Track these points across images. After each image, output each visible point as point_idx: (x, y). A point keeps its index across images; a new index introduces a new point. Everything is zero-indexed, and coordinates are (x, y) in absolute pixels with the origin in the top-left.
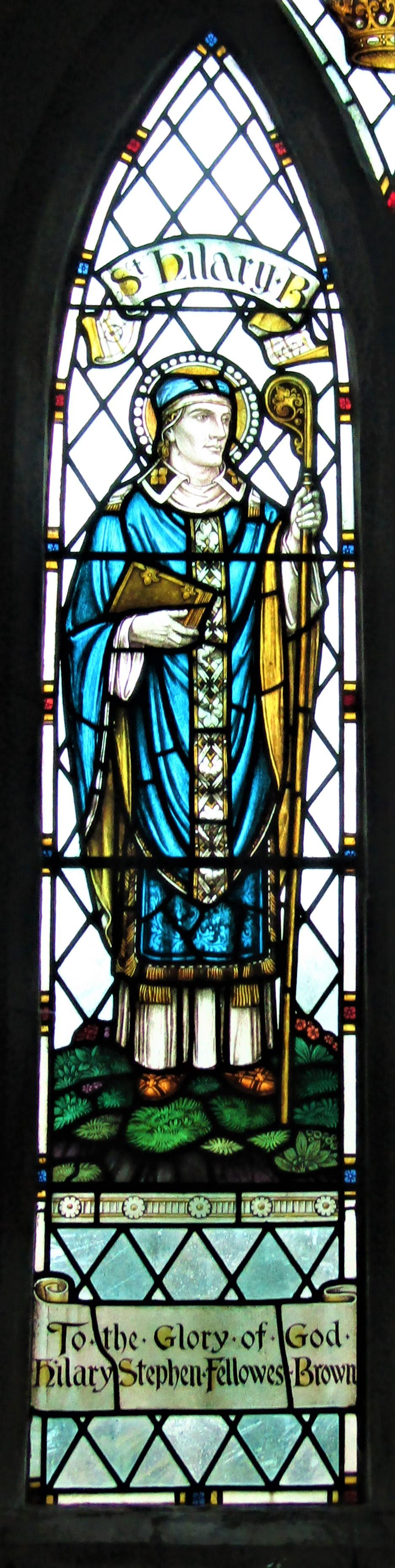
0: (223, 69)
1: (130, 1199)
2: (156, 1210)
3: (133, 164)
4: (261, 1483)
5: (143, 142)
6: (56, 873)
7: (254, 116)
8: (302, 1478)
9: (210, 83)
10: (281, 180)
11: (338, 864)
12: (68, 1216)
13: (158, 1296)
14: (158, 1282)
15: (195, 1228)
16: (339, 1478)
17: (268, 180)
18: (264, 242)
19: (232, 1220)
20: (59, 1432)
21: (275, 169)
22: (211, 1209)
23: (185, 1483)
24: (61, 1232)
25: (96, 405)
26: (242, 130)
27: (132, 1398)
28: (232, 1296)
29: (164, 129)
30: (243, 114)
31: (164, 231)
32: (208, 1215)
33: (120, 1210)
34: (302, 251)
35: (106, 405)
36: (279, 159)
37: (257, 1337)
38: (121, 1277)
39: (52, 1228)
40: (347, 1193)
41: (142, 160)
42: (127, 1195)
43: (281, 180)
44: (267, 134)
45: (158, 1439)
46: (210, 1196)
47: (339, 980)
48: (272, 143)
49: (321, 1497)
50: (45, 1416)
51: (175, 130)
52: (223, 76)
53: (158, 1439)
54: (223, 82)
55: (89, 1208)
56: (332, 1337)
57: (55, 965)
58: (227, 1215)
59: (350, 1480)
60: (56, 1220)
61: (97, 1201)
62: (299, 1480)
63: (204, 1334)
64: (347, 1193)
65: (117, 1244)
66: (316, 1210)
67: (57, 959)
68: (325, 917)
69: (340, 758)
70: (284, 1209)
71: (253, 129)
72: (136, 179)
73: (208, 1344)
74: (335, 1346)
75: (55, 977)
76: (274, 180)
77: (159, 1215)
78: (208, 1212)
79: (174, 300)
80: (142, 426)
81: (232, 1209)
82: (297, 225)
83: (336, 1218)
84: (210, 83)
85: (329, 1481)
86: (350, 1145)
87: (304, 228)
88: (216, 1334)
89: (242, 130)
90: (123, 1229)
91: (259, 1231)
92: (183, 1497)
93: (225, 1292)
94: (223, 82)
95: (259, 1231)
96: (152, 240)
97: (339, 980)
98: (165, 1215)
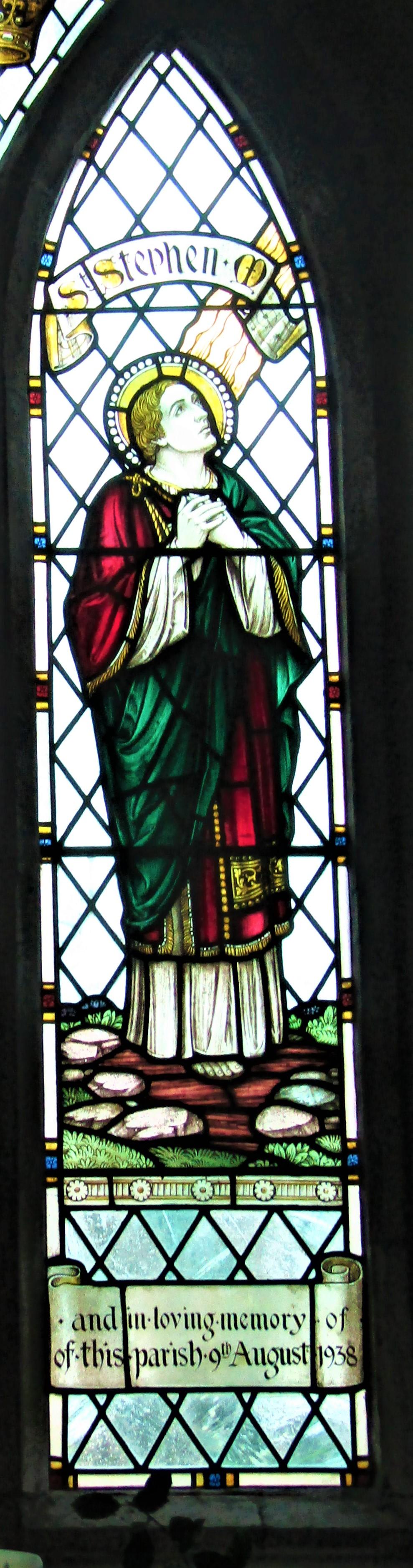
0: (174, 65)
1: (199, 1182)
2: (285, 1193)
3: (91, 162)
4: (131, 1466)
5: (101, 138)
6: (56, 862)
7: (210, 110)
8: (306, 1462)
9: (162, 80)
10: (244, 172)
11: (329, 850)
12: (74, 1198)
13: (170, 1276)
14: (241, 1263)
15: (204, 1211)
16: (353, 1461)
17: (230, 173)
18: (221, 233)
19: (227, 1202)
20: (82, 1411)
21: (236, 161)
22: (151, 1191)
23: (206, 1465)
24: (74, 1214)
25: (274, 407)
26: (199, 125)
27: (148, 1376)
28: (170, 1276)
29: (120, 127)
30: (199, 109)
32: (272, 1198)
33: (252, 1194)
34: (271, 242)
35: (278, 406)
36: (241, 151)
37: (339, 1319)
38: (134, 1258)
40: (350, 1178)
41: (101, 158)
42: (135, 1178)
43: (244, 172)
44: (226, 129)
46: (273, 1178)
47: (336, 964)
48: (233, 137)
49: (335, 1480)
50: (65, 1393)
51: (132, 126)
52: (174, 71)
54: (174, 78)
55: (226, 1191)
56: (109, 1322)
57: (59, 951)
58: (221, 1197)
59: (363, 1465)
60: (68, 1203)
61: (233, 1184)
62: (114, 1465)
63: (284, 1316)
64: (350, 1178)
65: (270, 1225)
66: (193, 1193)
67: (61, 945)
68: (320, 902)
69: (326, 742)
70: (180, 1192)
71: (210, 123)
72: (96, 182)
73: (287, 1325)
74: (112, 1329)
75: (59, 965)
76: (236, 173)
77: (165, 1197)
78: (272, 1193)
79: (141, 298)
80: (227, 426)
81: (240, 1191)
82: (265, 216)
83: (340, 1203)
84: (162, 80)
85: (342, 1464)
86: (352, 1131)
87: (272, 218)
88: (296, 1317)
89: (199, 125)
90: (135, 1211)
91: (264, 1213)
93: (234, 1272)
94: (174, 78)
95: (264, 1213)
96: (121, 237)
97: (336, 964)
98: (177, 1197)
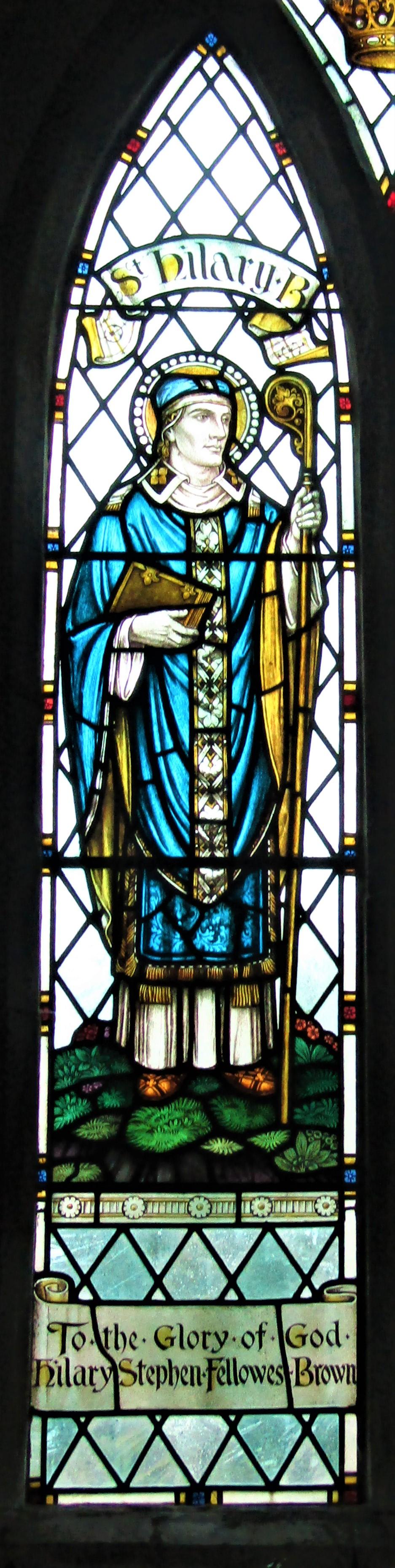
0: (223, 69)
1: (130, 1199)
2: (156, 1210)
3: (133, 164)
4: (261, 1483)
5: (143, 142)
7: (254, 116)
8: (302, 1478)
9: (210, 83)
10: (281, 180)
11: (338, 864)
12: (68, 1216)
13: (158, 1296)
14: (158, 1282)
15: (195, 1228)
16: (339, 1478)
17: (268, 180)
18: (264, 242)
19: (232, 1220)
20: (59, 1432)
21: (275, 169)
22: (211, 1209)
23: (185, 1483)
24: (61, 1232)
25: (96, 405)
26: (242, 130)
27: (132, 1398)
28: (232, 1296)
29: (164, 129)
30: (243, 114)
32: (208, 1215)
33: (120, 1210)
34: (302, 251)
35: (106, 405)
36: (279, 159)
37: (257, 1337)
38: (121, 1277)
40: (347, 1193)
41: (142, 160)
42: (127, 1195)
43: (281, 180)
44: (267, 134)
45: (158, 1439)
46: (210, 1196)
47: (339, 980)
48: (272, 143)
49: (321, 1497)
50: (45, 1416)
51: (175, 130)
52: (223, 76)
53: (158, 1439)
54: (223, 82)
55: (89, 1208)
56: (332, 1337)
57: (55, 965)
58: (227, 1215)
59: (350, 1480)
60: (56, 1220)
61: (97, 1201)
62: (299, 1480)
63: (204, 1334)
64: (347, 1193)
65: (117, 1244)
66: (316, 1210)
67: (57, 959)
68: (325, 917)
69: (340, 758)
70: (284, 1209)
71: (253, 129)
73: (208, 1344)
74: (335, 1346)
76: (274, 180)
77: (159, 1215)
78: (208, 1212)
81: (232, 1209)
82: (297, 225)
83: (336, 1218)
84: (210, 83)
85: (329, 1481)
86: (350, 1145)
87: (304, 228)
88: (216, 1334)
89: (242, 130)
90: (123, 1229)
91: (259, 1231)
93: (225, 1292)
94: (223, 82)
95: (259, 1231)
96: (152, 240)
97: (339, 980)
98: (165, 1215)
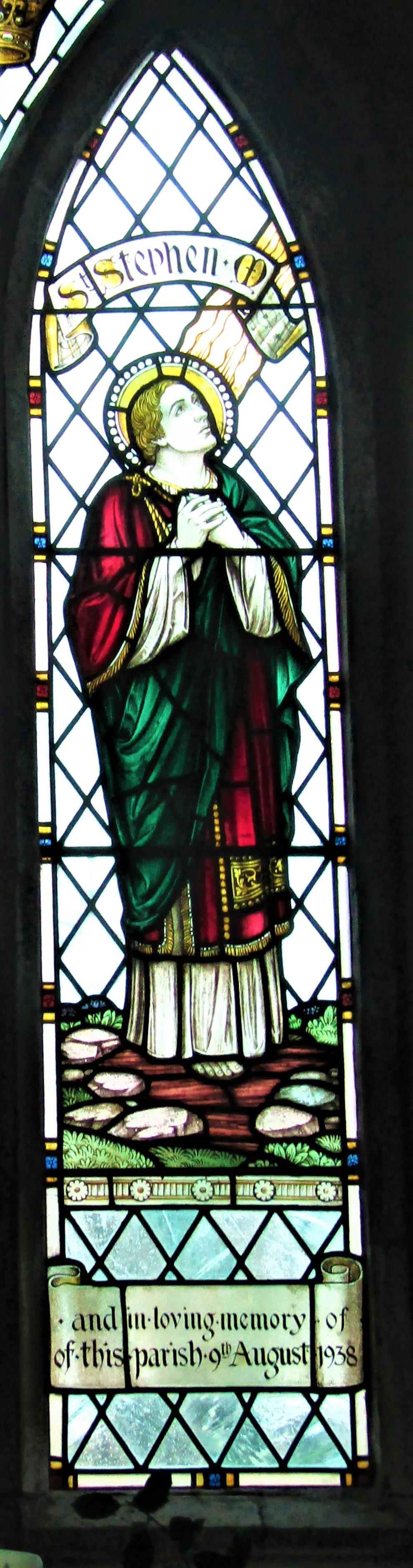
0: (174, 65)
1: (199, 1182)
2: (285, 1193)
3: (91, 162)
4: (131, 1466)
5: (101, 138)
6: (56, 862)
7: (210, 110)
8: (306, 1462)
9: (162, 80)
10: (244, 172)
11: (329, 850)
12: (74, 1198)
13: (170, 1276)
14: (241, 1263)
15: (204, 1211)
16: (353, 1461)
17: (230, 173)
18: (221, 233)
19: (227, 1202)
20: (82, 1411)
21: (236, 161)
22: (151, 1191)
23: (206, 1465)
24: (74, 1214)
25: (274, 407)
26: (199, 125)
27: (148, 1376)
28: (170, 1276)
29: (120, 127)
30: (199, 109)
31: (206, 234)
32: (272, 1198)
33: (252, 1194)
34: (271, 242)
35: (278, 406)
36: (241, 151)
37: (339, 1319)
38: (134, 1258)
39: (65, 1212)
40: (350, 1178)
41: (101, 158)
42: (135, 1178)
43: (244, 172)
44: (226, 129)
45: (175, 1421)
46: (273, 1178)
47: (336, 964)
48: (233, 137)
49: (335, 1480)
50: (65, 1393)
51: (132, 126)
52: (174, 71)
53: (175, 1421)
54: (174, 78)
55: (226, 1191)
56: (109, 1322)
57: (59, 951)
58: (221, 1197)
59: (363, 1465)
60: (68, 1203)
61: (233, 1184)
62: (114, 1465)
63: (284, 1316)
64: (350, 1178)
65: (270, 1225)
66: (193, 1193)
67: (61, 945)
68: (320, 902)
69: (326, 742)
70: (180, 1192)
71: (210, 123)
73: (287, 1325)
74: (112, 1329)
76: (236, 173)
77: (165, 1197)
78: (272, 1193)
80: (227, 426)
81: (240, 1191)
82: (265, 216)
83: (340, 1203)
84: (162, 80)
85: (342, 1464)
86: (352, 1131)
87: (272, 218)
88: (296, 1317)
89: (199, 125)
90: (135, 1211)
91: (264, 1213)
92: (200, 1481)
93: (234, 1272)
94: (174, 78)
95: (264, 1213)
96: (121, 237)
97: (336, 964)
98: (177, 1197)
